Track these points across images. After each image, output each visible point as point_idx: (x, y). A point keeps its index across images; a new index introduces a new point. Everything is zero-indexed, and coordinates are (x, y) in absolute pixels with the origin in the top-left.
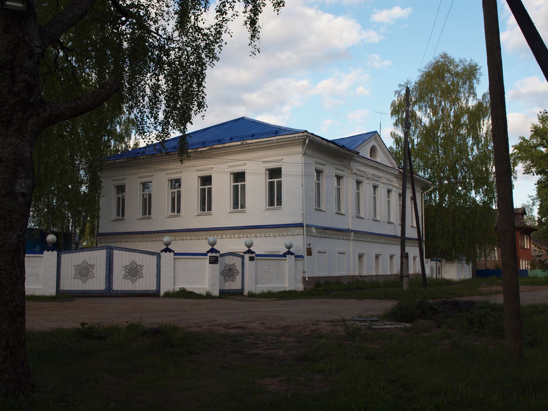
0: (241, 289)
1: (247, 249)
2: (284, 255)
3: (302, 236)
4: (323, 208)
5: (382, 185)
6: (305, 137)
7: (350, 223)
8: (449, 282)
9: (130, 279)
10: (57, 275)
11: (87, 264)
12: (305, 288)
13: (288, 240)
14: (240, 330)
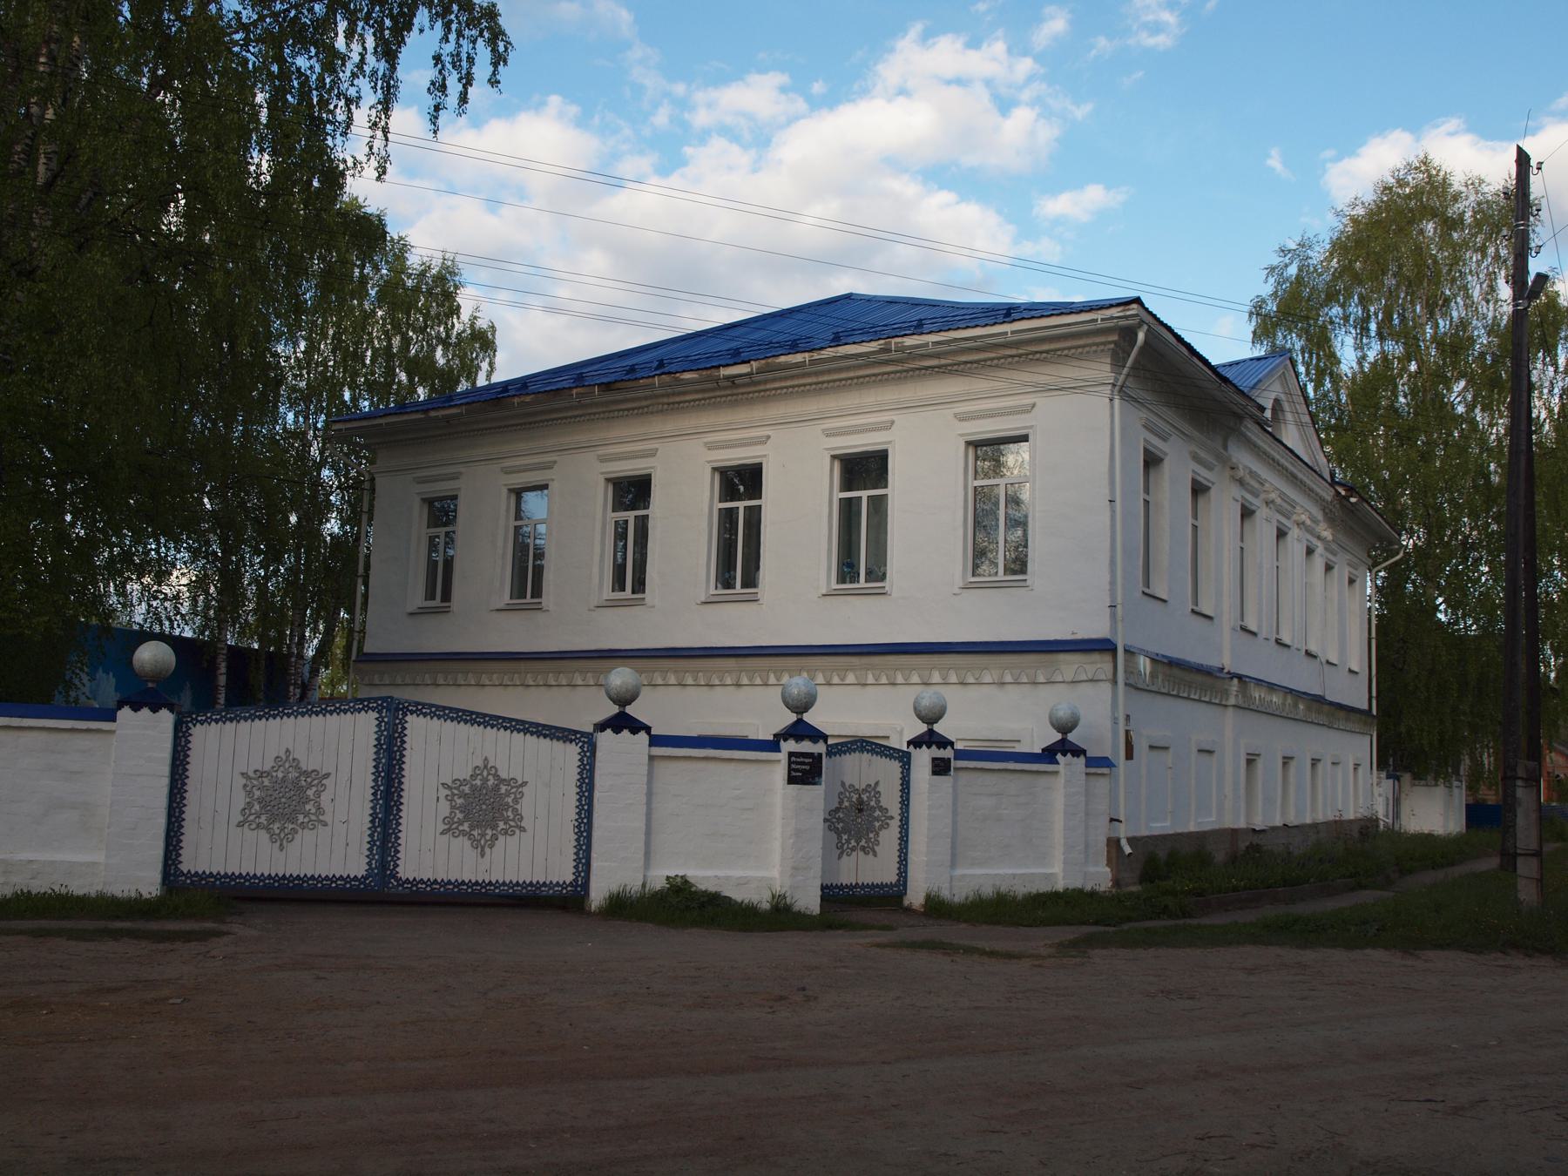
1: (923, 728)
3: (1107, 687)
9: (469, 835)
11: (297, 767)
12: (1116, 882)
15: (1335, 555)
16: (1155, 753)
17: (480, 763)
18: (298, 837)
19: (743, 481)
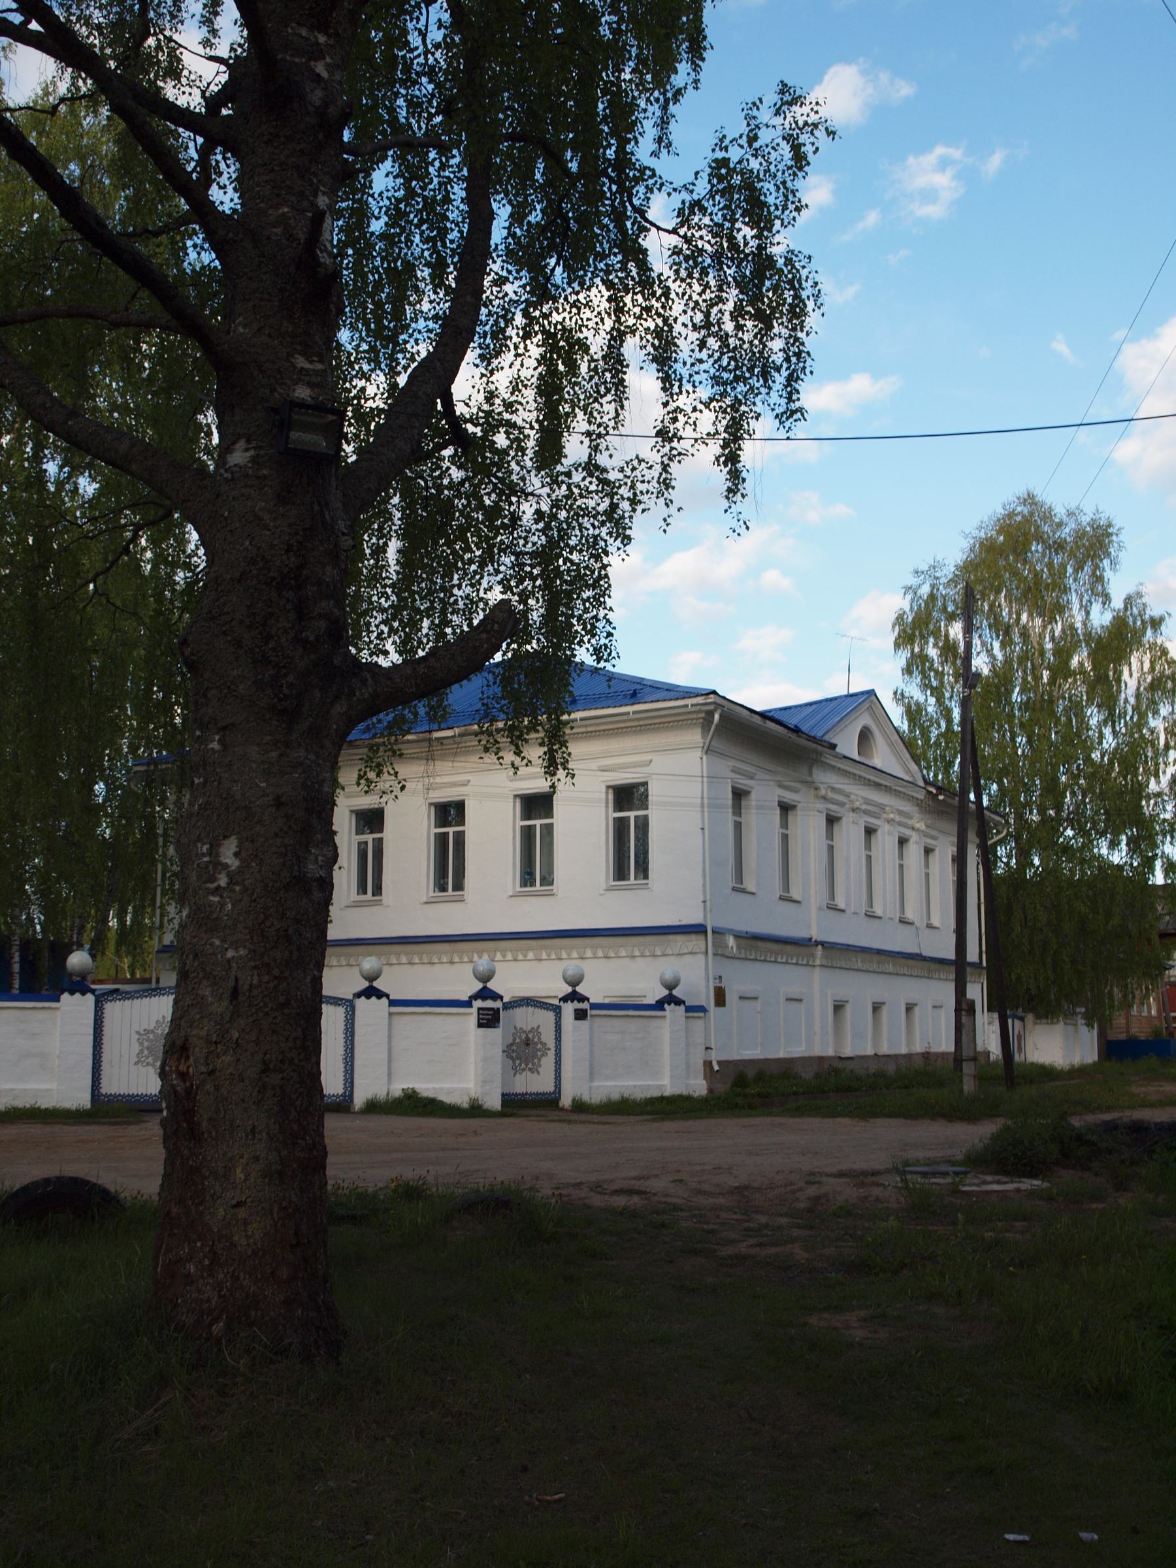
0: (554, 1093)
2: (660, 1005)
3: (701, 957)
4: (750, 885)
5: (887, 827)
6: (712, 707)
7: (814, 926)
8: (1046, 1073)
10: (94, 1055)
12: (710, 1090)
13: (668, 967)
14: (636, 1199)
15: (935, 838)
16: (746, 1003)
19: (450, 813)
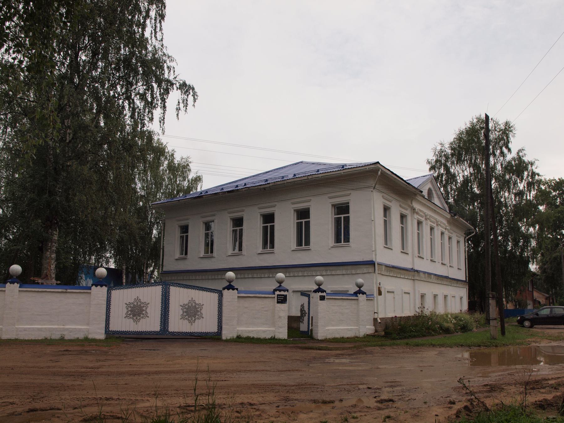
1: (317, 287)
15: (452, 234)
17: (190, 299)
18: (141, 321)
